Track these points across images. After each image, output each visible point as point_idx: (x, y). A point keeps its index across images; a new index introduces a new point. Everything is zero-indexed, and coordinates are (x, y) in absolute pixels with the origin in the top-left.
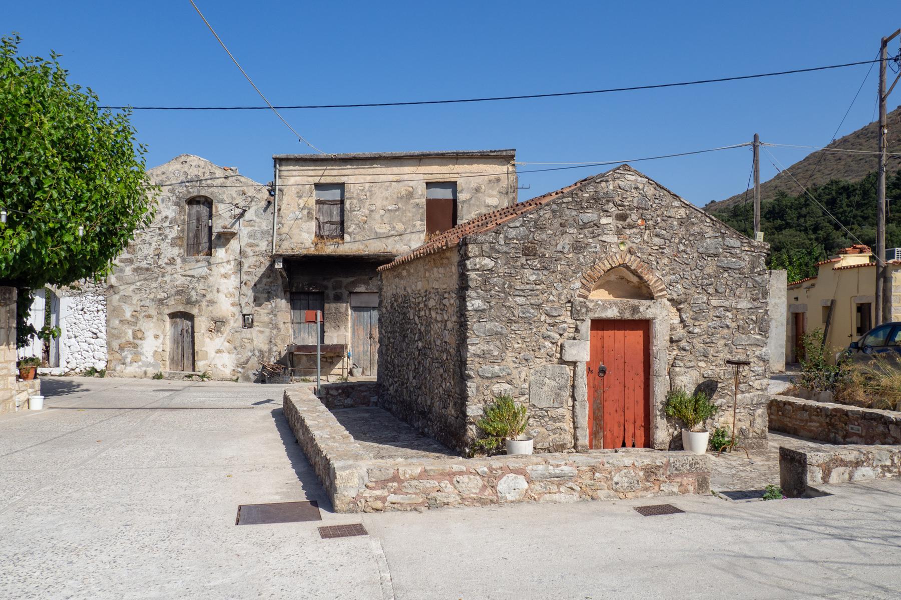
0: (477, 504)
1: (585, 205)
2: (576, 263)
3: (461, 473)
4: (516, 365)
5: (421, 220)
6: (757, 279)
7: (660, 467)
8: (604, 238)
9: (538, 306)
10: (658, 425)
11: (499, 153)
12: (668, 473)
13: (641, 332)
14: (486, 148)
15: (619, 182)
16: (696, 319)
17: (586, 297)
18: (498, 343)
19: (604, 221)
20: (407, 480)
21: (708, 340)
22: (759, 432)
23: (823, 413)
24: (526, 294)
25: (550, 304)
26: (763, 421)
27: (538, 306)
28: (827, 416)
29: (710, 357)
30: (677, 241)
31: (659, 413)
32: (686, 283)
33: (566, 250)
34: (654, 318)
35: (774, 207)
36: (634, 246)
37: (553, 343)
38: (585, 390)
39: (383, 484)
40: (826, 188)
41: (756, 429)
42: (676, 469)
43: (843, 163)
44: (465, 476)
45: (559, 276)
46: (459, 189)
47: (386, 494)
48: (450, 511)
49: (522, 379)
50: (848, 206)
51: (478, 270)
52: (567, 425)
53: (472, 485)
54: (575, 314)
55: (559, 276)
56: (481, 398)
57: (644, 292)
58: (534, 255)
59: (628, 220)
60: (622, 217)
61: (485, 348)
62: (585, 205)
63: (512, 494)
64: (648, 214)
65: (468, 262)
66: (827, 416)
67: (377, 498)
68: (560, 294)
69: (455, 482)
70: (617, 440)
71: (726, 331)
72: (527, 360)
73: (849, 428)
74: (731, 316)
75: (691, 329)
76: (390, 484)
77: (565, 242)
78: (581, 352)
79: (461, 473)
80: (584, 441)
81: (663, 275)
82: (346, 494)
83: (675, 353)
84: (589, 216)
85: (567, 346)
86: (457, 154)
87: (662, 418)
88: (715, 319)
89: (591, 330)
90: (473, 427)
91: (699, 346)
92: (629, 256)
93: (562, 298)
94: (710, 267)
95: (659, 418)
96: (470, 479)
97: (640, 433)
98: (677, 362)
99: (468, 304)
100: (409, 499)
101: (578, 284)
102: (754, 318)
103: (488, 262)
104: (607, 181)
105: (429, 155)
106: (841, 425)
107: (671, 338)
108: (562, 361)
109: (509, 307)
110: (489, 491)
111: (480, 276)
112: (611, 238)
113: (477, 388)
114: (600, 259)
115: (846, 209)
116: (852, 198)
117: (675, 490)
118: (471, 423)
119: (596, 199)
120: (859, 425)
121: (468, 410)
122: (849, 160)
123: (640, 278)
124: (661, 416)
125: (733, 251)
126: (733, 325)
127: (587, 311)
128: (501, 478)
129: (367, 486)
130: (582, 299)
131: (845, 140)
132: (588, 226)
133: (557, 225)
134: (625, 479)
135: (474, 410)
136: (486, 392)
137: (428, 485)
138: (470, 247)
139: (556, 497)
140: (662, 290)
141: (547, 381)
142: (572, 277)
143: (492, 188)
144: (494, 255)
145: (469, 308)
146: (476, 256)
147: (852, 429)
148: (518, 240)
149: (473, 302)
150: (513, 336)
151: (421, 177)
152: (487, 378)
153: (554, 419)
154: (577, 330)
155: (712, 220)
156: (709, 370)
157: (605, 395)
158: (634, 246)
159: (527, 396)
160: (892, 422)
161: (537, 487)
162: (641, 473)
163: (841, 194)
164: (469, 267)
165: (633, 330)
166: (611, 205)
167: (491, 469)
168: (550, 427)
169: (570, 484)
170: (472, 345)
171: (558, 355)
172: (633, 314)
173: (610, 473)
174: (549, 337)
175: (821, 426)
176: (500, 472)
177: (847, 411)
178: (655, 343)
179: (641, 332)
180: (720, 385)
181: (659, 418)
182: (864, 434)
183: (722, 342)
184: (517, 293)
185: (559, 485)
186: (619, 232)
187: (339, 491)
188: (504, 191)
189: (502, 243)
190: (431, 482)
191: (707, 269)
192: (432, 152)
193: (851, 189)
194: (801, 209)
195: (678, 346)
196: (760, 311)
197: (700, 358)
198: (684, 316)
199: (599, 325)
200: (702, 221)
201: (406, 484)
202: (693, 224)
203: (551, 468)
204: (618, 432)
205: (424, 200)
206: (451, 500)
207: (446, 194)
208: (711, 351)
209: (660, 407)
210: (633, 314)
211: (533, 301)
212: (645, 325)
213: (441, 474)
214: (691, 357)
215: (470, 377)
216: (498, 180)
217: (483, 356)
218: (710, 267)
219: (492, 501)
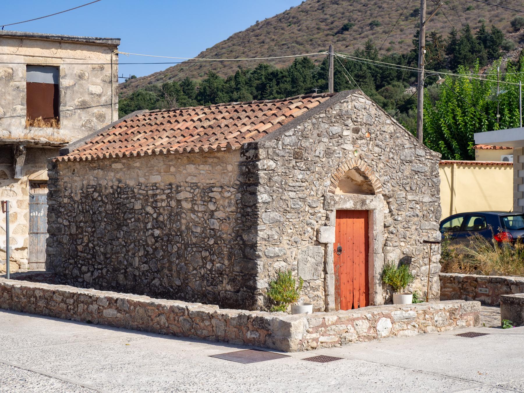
0: (366, 340)
1: (334, 120)
2: (327, 165)
3: (358, 319)
4: (289, 247)
5: (22, 105)
6: (434, 180)
7: (457, 309)
8: (345, 146)
9: (303, 200)
10: (377, 291)
11: (104, 41)
12: (461, 313)
13: (363, 219)
14: (92, 35)
15: (354, 103)
16: (399, 210)
17: (333, 193)
18: (277, 229)
19: (345, 133)
20: (330, 325)
21: (406, 226)
22: (435, 294)
23: (456, 281)
24: (296, 190)
25: (311, 198)
26: (438, 286)
27: (303, 200)
28: (459, 283)
29: (407, 238)
30: (388, 150)
31: (378, 282)
32: (393, 182)
33: (321, 156)
34: (375, 209)
35: (205, 89)
36: (363, 153)
37: (312, 228)
38: (333, 265)
39: (316, 329)
40: (255, 72)
41: (433, 292)
42: (465, 311)
43: (266, 46)
44: (360, 321)
45: (317, 176)
46: (62, 74)
47: (319, 336)
48: (353, 345)
49: (293, 258)
50: (278, 93)
51: (265, 170)
52: (321, 293)
53: (363, 326)
54: (325, 205)
55: (317, 176)
56: (266, 274)
57: (365, 188)
58: (301, 159)
59: (360, 133)
60: (356, 131)
61: (270, 233)
62: (334, 120)
63: (385, 332)
64: (372, 128)
65: (259, 163)
66: (459, 283)
67: (313, 340)
68: (317, 190)
69: (355, 325)
70: (349, 304)
71: (416, 219)
72: (296, 242)
73: (478, 290)
74: (419, 208)
75: (396, 217)
76: (320, 329)
77: (320, 149)
78: (329, 236)
79: (358, 319)
80: (332, 305)
81: (380, 176)
82: (297, 338)
83: (386, 235)
84: (336, 129)
85: (322, 230)
86: (62, 38)
87: (379, 286)
88: (410, 209)
89: (336, 218)
90: (261, 297)
91: (401, 230)
92: (360, 160)
93: (319, 193)
94: (407, 170)
95: (378, 285)
96: (363, 322)
97: (363, 298)
98: (388, 242)
99: (259, 197)
100: (331, 339)
101: (328, 183)
102: (433, 209)
103: (271, 163)
104: (348, 102)
105: (32, 36)
106: (471, 289)
107: (385, 224)
108: (318, 243)
109: (285, 200)
110: (372, 331)
111: (266, 174)
112: (349, 147)
113: (264, 265)
114: (342, 163)
115: (276, 95)
116: (281, 85)
117: (464, 324)
118: (260, 294)
119: (340, 116)
120: (486, 287)
121: (258, 284)
122: (272, 44)
123: (366, 178)
124: (379, 283)
125: (421, 159)
126: (420, 214)
127: (335, 203)
128: (378, 321)
129: (308, 332)
130: (331, 194)
131: (267, 23)
132: (335, 136)
133: (315, 135)
134: (440, 318)
135: (262, 284)
136: (270, 269)
137: (341, 328)
138: (261, 150)
139: (406, 332)
140: (379, 188)
141: (309, 258)
142: (325, 176)
143: (96, 76)
144: (275, 158)
145: (260, 201)
146: (264, 159)
147: (481, 290)
148: (290, 146)
149: (262, 196)
150: (288, 223)
151: (22, 59)
152: (271, 257)
153: (314, 289)
154: (327, 218)
155: (409, 135)
156: (407, 248)
157: (342, 269)
158: (363, 153)
159: (296, 271)
160: (513, 283)
161: (397, 326)
162: (448, 314)
163: (271, 80)
164: (260, 167)
165: (358, 218)
166: (350, 121)
167: (373, 315)
168: (311, 296)
169: (414, 323)
170: (261, 230)
171: (315, 239)
172: (362, 206)
173: (433, 314)
174: (311, 224)
175: (454, 290)
176: (378, 317)
177: (477, 278)
178: (375, 228)
179: (363, 219)
180: (413, 259)
181: (378, 285)
182: (490, 294)
183: (414, 227)
184: (290, 189)
185: (408, 324)
186: (354, 143)
187: (293, 336)
188: (108, 80)
189: (281, 148)
190: (343, 325)
191: (405, 172)
192: (36, 34)
193: (280, 75)
194: (232, 92)
195: (388, 230)
196: (436, 204)
197: (402, 240)
198: (392, 208)
199: (342, 214)
200: (403, 136)
201: (329, 328)
202: (398, 137)
203: (404, 312)
204: (349, 298)
205: (25, 83)
206: (353, 338)
207: (48, 78)
208: (408, 234)
209: (379, 277)
210: (362, 206)
211: (300, 196)
212: (365, 215)
213: (348, 320)
214: (396, 239)
215: (259, 257)
216: (102, 69)
217: (268, 239)
218: (407, 170)
219: (374, 337)
